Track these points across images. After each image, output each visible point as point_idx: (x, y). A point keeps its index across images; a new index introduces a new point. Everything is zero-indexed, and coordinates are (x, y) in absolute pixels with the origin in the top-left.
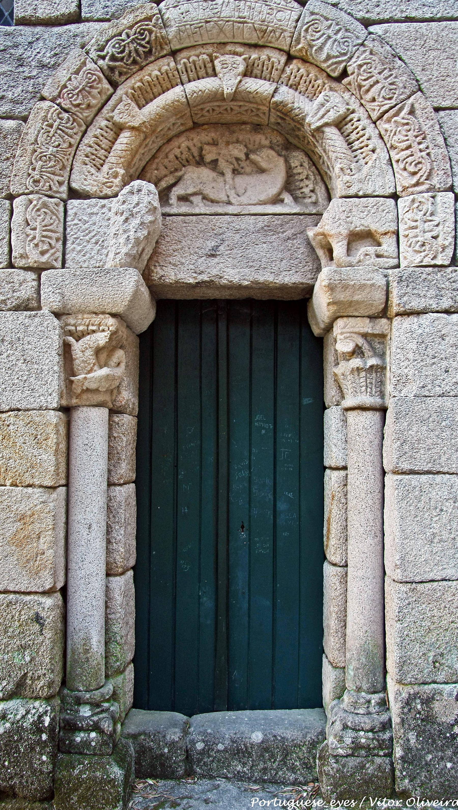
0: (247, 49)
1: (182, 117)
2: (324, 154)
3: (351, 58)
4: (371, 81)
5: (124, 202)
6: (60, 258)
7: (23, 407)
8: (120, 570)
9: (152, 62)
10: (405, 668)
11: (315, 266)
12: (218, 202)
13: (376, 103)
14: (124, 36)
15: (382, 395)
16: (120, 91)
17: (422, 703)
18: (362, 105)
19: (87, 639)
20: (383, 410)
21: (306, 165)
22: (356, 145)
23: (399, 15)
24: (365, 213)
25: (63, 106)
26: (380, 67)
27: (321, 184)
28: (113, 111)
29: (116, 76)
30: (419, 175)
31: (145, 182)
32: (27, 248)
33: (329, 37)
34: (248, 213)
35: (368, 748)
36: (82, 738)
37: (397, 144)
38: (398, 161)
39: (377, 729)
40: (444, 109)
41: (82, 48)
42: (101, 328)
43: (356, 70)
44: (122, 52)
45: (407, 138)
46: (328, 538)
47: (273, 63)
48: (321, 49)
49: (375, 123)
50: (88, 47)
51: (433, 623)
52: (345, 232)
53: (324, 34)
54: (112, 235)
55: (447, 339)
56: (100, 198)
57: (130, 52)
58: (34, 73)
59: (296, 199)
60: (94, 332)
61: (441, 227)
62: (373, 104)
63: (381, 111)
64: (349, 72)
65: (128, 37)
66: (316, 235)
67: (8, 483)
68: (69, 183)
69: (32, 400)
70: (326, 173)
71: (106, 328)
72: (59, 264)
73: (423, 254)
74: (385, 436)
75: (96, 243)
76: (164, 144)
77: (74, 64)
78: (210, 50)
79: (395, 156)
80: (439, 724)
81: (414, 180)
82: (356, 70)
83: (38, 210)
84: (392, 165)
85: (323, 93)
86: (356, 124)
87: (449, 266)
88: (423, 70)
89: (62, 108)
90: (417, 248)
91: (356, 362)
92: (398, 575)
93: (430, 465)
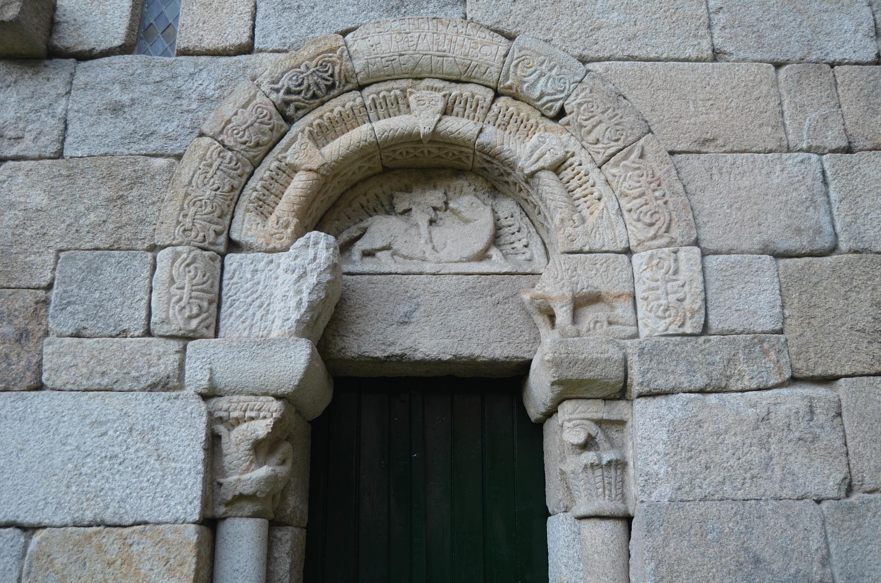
0: (447, 83)
1: (370, 160)
2: (540, 203)
3: (568, 96)
4: (593, 121)
5: (296, 257)
6: (213, 326)
7: (152, 520)
9: (335, 97)
12: (411, 259)
13: (600, 145)
14: (303, 68)
15: (624, 498)
16: (296, 128)
18: (583, 147)
20: (628, 520)
21: (517, 215)
22: (578, 193)
23: (620, 53)
24: (594, 272)
26: (602, 107)
28: (287, 151)
29: (290, 111)
30: (656, 227)
31: (323, 234)
32: (171, 312)
33: (542, 75)
34: (447, 272)
37: (628, 192)
38: (630, 211)
40: (680, 153)
41: (253, 80)
42: (262, 414)
43: (575, 109)
44: (300, 85)
45: (639, 184)
48: (533, 85)
49: (600, 168)
50: (260, 79)
54: (280, 297)
55: (706, 425)
56: (266, 252)
57: (309, 86)
59: (505, 256)
60: (252, 419)
61: (687, 288)
62: (596, 146)
63: (606, 154)
64: (567, 111)
65: (308, 68)
66: (533, 299)
68: (228, 234)
71: (269, 415)
72: (212, 332)
73: (668, 320)
75: (260, 307)
76: (347, 190)
77: (240, 98)
78: (404, 83)
79: (626, 205)
81: (652, 231)
82: (575, 109)
84: (622, 215)
85: (537, 135)
86: (578, 169)
87: (701, 335)
89: (224, 146)
90: (660, 313)
91: (589, 457)
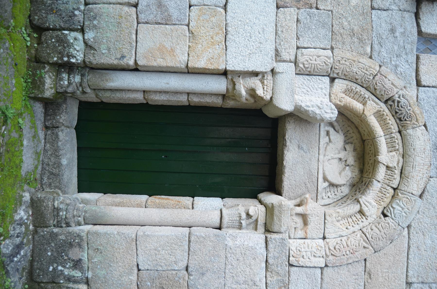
0: (401, 168)
1: (368, 135)
3: (393, 219)
6: (300, 73)
8: (146, 97)
9: (396, 121)
10: (95, 235)
11: (291, 197)
13: (370, 230)
14: (409, 108)
17: (78, 242)
19: (113, 81)
20: (220, 228)
21: (342, 194)
22: (350, 220)
23: (411, 243)
24: (316, 223)
25: (376, 76)
27: (332, 201)
29: (390, 103)
30: (334, 250)
33: (403, 209)
35: (58, 215)
36: (65, 77)
38: (341, 240)
39: (66, 220)
40: (365, 263)
42: (265, 92)
43: (386, 222)
44: (402, 107)
46: (160, 198)
47: (392, 181)
48: (398, 205)
49: (360, 230)
50: (405, 90)
51: (116, 249)
52: (307, 213)
53: (405, 206)
55: (254, 261)
56: (330, 93)
57: (401, 111)
58: (393, 63)
60: (264, 88)
63: (366, 233)
64: (386, 218)
65: (409, 110)
66: (306, 198)
67: (190, 44)
69: (231, 57)
70: (337, 204)
71: (265, 95)
73: (295, 251)
74: (207, 229)
76: (355, 125)
78: (401, 150)
79: (344, 239)
80: (68, 250)
81: (332, 248)
82: (386, 222)
83: (325, 63)
84: (340, 237)
86: (360, 220)
87: (289, 263)
88: (385, 254)
90: (298, 248)
91: (244, 216)
92: (140, 233)
93: (193, 250)
